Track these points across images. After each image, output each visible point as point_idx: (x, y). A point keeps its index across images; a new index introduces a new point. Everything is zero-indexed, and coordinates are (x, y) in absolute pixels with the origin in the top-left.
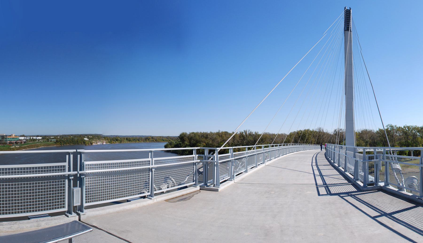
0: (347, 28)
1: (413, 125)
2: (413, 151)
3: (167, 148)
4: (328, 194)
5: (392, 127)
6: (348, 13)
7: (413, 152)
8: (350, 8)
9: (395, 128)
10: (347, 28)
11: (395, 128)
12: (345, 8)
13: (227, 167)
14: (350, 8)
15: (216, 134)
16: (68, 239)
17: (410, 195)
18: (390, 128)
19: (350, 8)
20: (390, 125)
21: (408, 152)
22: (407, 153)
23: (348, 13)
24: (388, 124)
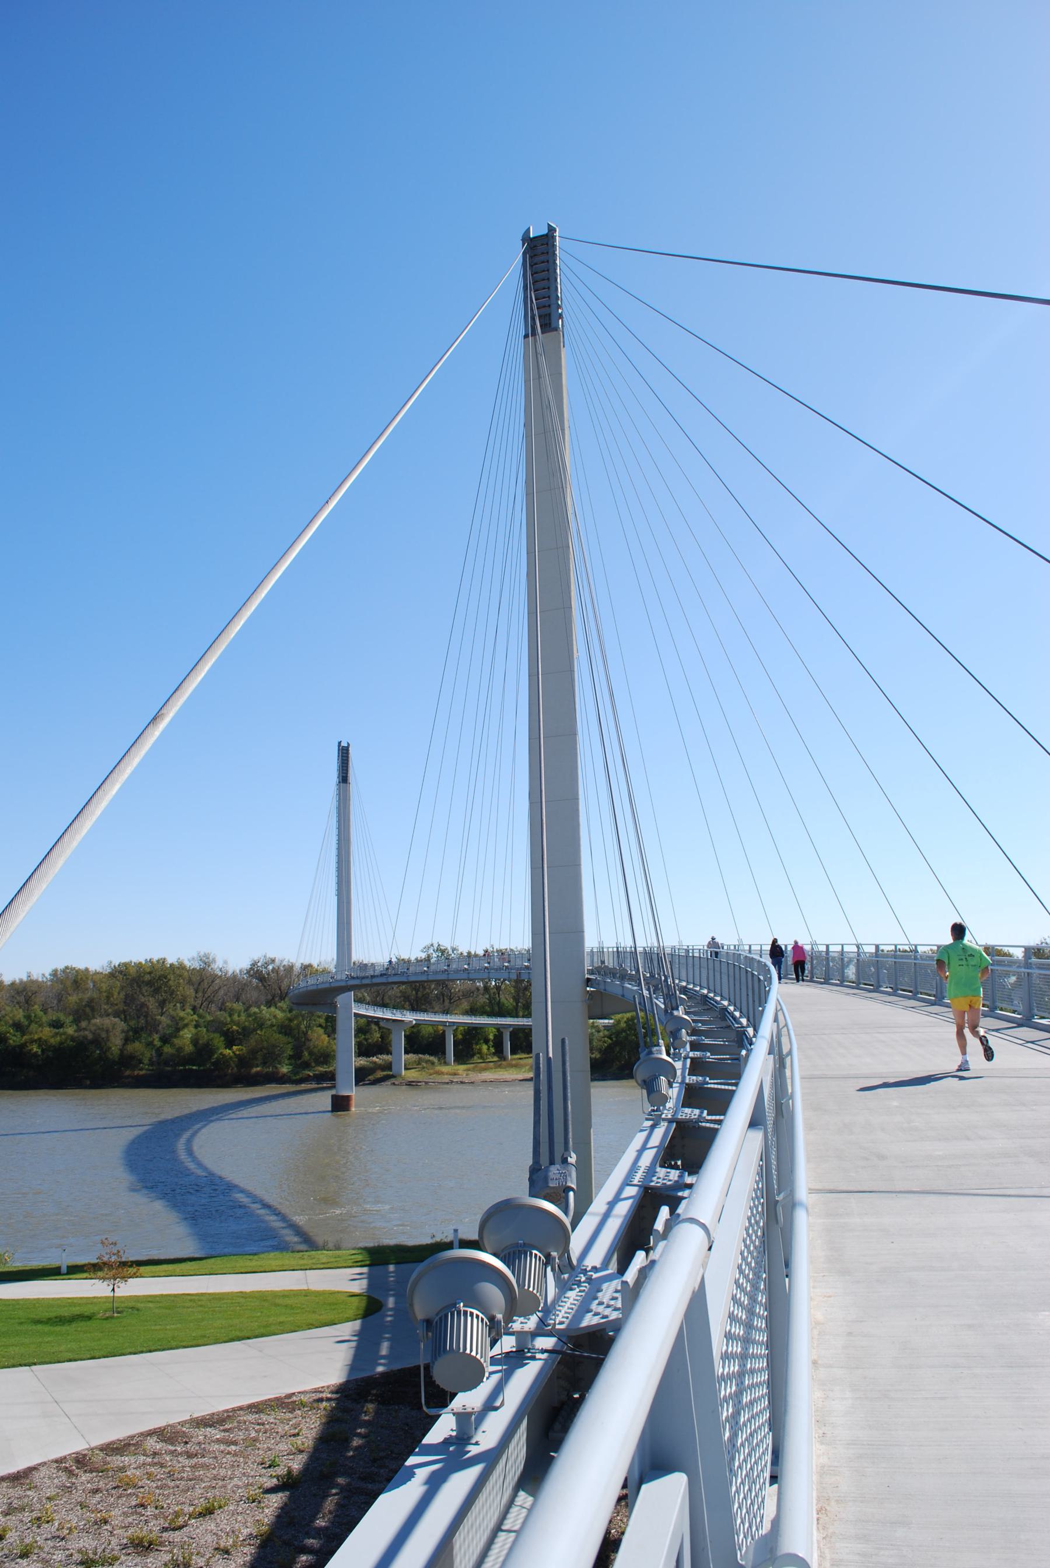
0: (344, 778)
1: (517, 948)
2: (511, 1029)
3: (425, 1011)
4: (861, 945)
5: (443, 952)
6: (344, 754)
7: (510, 1032)
8: (348, 743)
9: (453, 955)
10: (344, 778)
11: (453, 955)
12: (340, 743)
13: (1044, 995)
14: (348, 744)
15: (134, 980)
16: (1023, 949)
17: (411, 1457)
18: (434, 955)
19: (348, 743)
20: (436, 946)
21: (495, 1036)
22: (491, 1037)
23: (344, 754)
24: (428, 943)
